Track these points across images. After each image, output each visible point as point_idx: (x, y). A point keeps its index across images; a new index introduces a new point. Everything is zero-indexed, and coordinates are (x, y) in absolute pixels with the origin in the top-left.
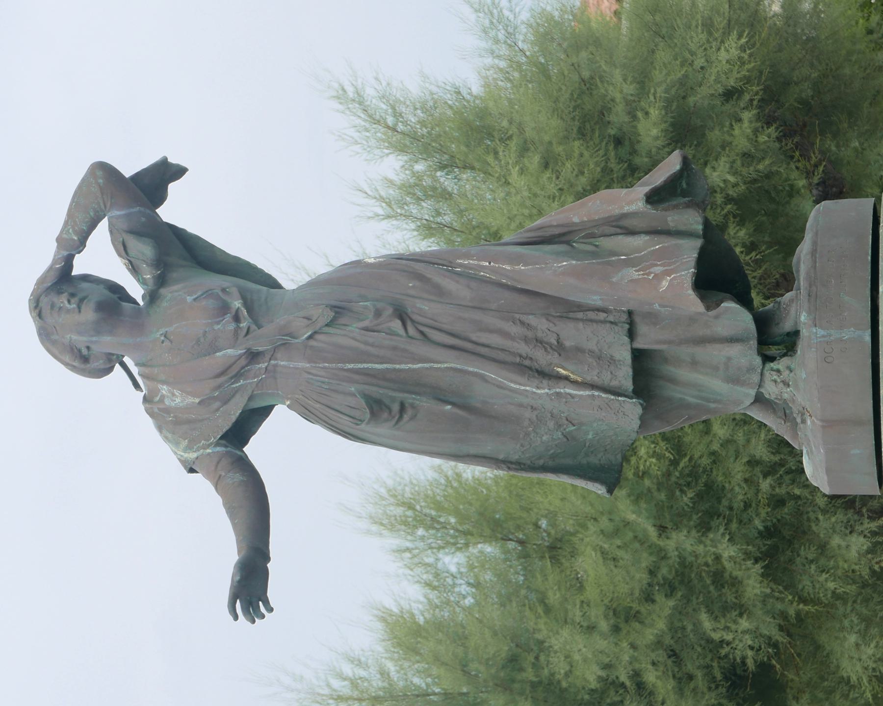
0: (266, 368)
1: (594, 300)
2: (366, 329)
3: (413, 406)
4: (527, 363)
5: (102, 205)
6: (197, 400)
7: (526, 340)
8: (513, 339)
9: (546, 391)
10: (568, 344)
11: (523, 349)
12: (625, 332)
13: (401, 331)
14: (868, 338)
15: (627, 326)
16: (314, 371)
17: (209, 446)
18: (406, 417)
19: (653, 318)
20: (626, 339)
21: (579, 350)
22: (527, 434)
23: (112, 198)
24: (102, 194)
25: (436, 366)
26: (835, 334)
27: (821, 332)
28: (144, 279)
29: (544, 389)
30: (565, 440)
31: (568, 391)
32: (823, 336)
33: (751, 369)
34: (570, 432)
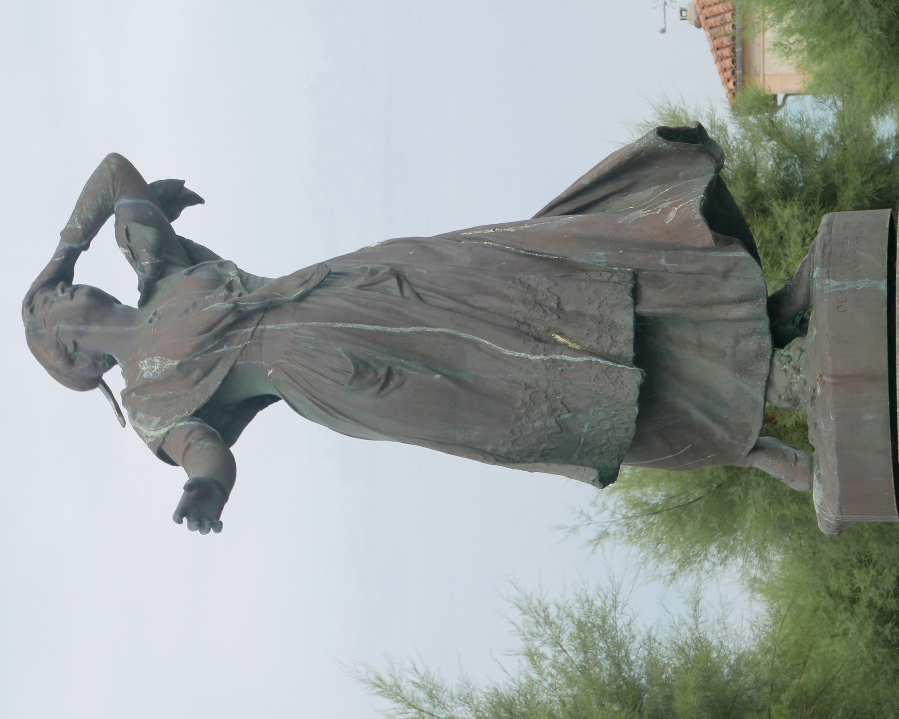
0: (253, 332)
1: (598, 258)
2: (361, 287)
3: (400, 374)
4: (524, 328)
5: (111, 190)
6: (176, 363)
7: (525, 301)
8: (511, 301)
9: (542, 357)
10: (568, 308)
12: (629, 291)
13: (397, 292)
14: (883, 286)
15: (631, 285)
16: (300, 331)
17: (182, 420)
18: (392, 384)
19: (658, 280)
20: (629, 300)
21: (580, 314)
22: (518, 418)
24: (113, 180)
25: (428, 330)
26: (849, 284)
27: (834, 283)
28: (142, 266)
29: (539, 355)
30: (559, 430)
31: (564, 357)
32: (836, 287)
33: (759, 356)
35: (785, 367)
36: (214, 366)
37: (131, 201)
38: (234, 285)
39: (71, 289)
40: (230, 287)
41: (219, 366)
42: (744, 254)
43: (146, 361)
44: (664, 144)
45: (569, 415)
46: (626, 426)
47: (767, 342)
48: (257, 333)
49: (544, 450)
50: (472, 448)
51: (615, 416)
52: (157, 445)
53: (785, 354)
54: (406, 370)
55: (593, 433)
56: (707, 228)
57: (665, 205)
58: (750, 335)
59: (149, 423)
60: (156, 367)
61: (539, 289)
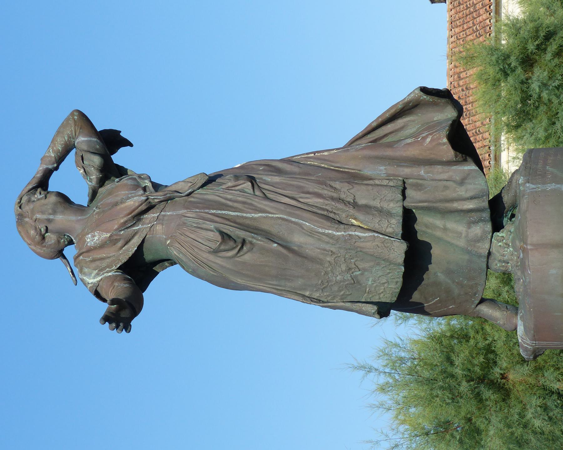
1: (381, 170)
4: (331, 215)
5: (73, 132)
6: (108, 235)
7: (332, 199)
11: (330, 205)
13: (251, 191)
15: (402, 188)
20: (400, 197)
22: (326, 273)
23: (81, 128)
25: (270, 215)
26: (540, 187)
27: (532, 186)
30: (353, 282)
31: (357, 233)
32: (533, 188)
34: (356, 276)
35: (500, 244)
36: (133, 237)
37: (86, 139)
38: (147, 189)
39: (46, 192)
40: (145, 189)
41: (136, 237)
42: (474, 167)
43: (90, 236)
44: (425, 97)
45: (360, 272)
46: (396, 280)
47: (489, 227)
48: (160, 217)
49: (343, 295)
50: (328, 218)
51: (389, 273)
52: (95, 288)
53: (500, 235)
54: (255, 241)
55: (375, 285)
56: (451, 148)
57: (424, 135)
58: (478, 222)
59: (90, 274)
60: (96, 238)
61: (342, 190)
